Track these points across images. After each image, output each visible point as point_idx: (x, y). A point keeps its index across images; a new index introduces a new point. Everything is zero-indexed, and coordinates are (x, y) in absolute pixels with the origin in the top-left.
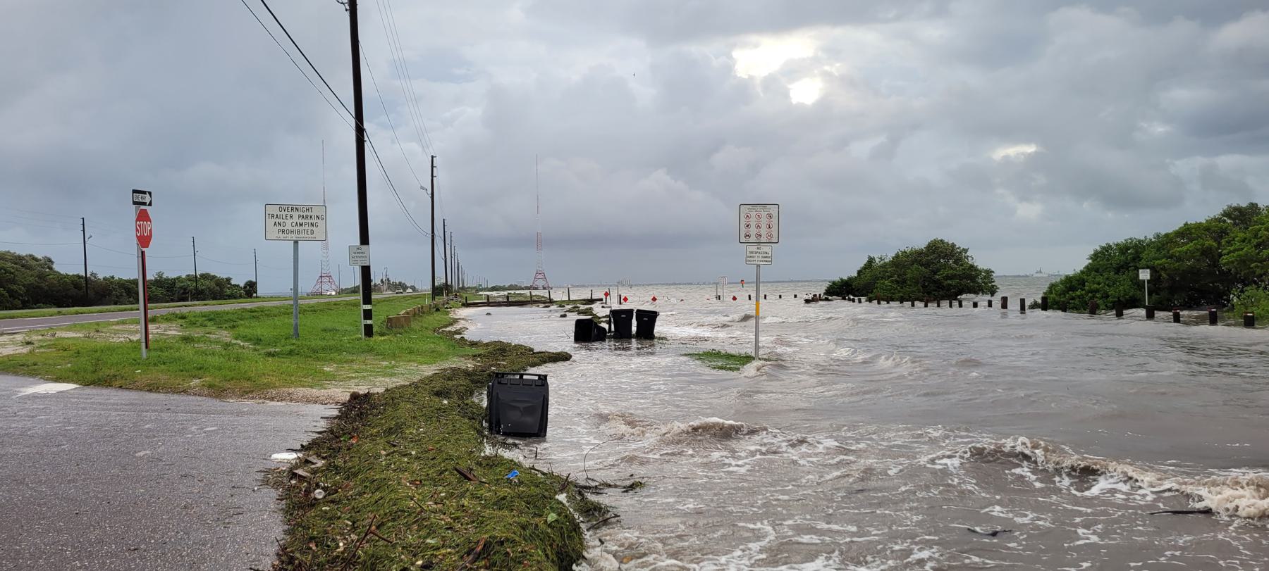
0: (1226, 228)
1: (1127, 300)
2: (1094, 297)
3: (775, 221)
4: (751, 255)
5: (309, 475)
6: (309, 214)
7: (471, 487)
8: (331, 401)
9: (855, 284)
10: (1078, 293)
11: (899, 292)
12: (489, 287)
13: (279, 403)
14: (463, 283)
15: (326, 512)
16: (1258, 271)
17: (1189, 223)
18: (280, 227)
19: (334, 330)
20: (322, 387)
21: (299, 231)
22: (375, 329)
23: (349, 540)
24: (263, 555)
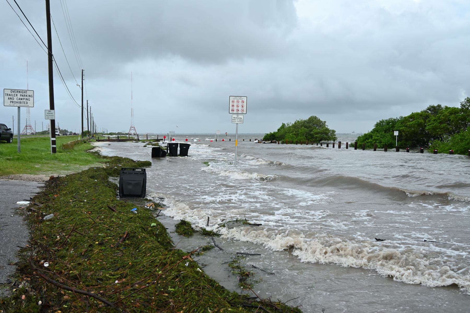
0: (428, 115)
1: (389, 144)
2: (376, 142)
3: (245, 104)
4: (234, 119)
5: (37, 210)
6: (26, 94)
7: (115, 214)
8: (41, 180)
9: (277, 135)
10: (370, 140)
11: (296, 139)
12: (108, 133)
13: (16, 181)
14: (96, 131)
15: (48, 224)
16: (439, 133)
17: (414, 113)
18: (11, 100)
19: (37, 150)
20: (35, 174)
21: (20, 102)
22: (57, 149)
23: (62, 235)
24: (21, 242)
